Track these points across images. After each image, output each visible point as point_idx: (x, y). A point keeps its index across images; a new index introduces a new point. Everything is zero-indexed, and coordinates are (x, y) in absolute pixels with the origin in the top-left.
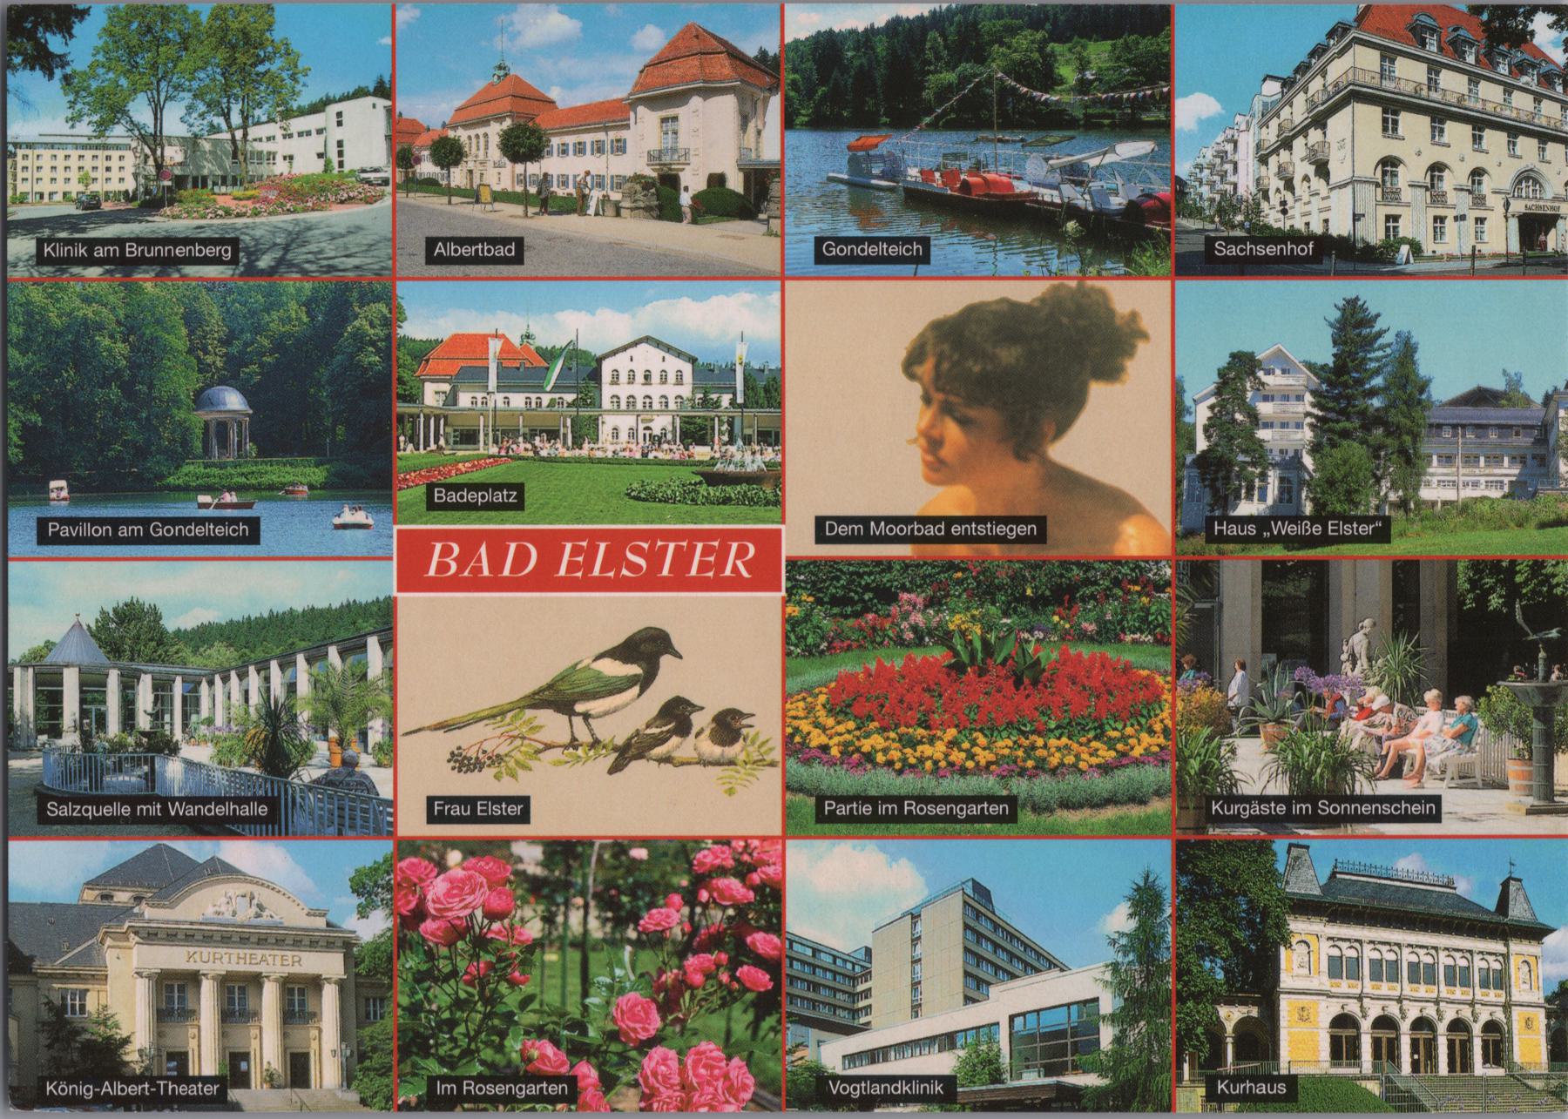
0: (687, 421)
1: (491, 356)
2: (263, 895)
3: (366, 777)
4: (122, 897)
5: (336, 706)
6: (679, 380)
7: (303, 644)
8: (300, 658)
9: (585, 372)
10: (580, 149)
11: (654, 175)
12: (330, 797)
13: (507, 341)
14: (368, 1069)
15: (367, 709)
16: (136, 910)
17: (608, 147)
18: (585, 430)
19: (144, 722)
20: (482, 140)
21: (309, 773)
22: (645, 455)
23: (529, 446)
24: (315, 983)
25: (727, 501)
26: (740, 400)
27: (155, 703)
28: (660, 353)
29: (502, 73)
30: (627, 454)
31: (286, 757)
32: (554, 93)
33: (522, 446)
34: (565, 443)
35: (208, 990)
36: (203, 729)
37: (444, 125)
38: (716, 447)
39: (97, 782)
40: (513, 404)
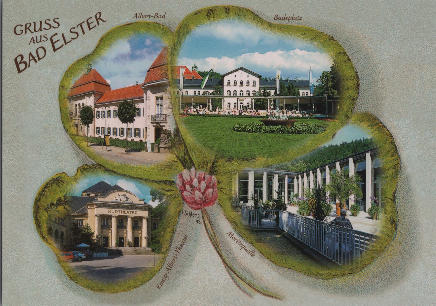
0: (257, 100)
1: (181, 75)
3: (348, 221)
5: (338, 188)
6: (254, 85)
7: (328, 161)
8: (327, 167)
9: (217, 81)
12: (337, 229)
13: (187, 70)
15: (349, 190)
18: (217, 104)
19: (275, 196)
21: (330, 219)
22: (240, 114)
23: (195, 110)
25: (273, 132)
26: (278, 92)
27: (279, 187)
28: (246, 74)
30: (233, 113)
31: (322, 212)
33: (193, 110)
34: (209, 109)
36: (295, 199)
38: (269, 111)
39: (259, 223)
40: (189, 94)
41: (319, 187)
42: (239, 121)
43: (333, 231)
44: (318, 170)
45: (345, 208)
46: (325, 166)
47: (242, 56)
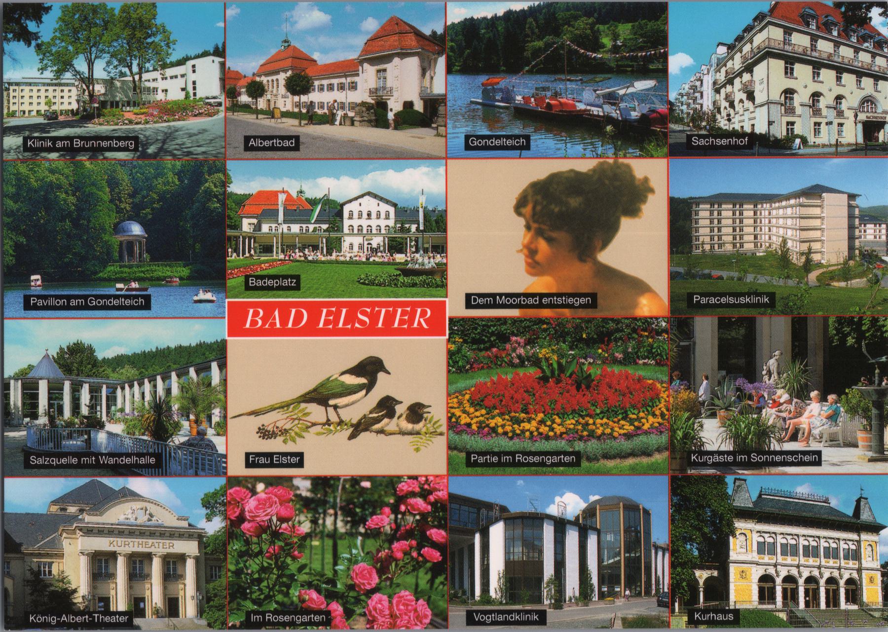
0: (392, 240)
1: (280, 203)
2: (152, 508)
4: (72, 510)
5: (194, 401)
6: (387, 217)
7: (175, 366)
9: (333, 212)
10: (331, 88)
11: (373, 102)
13: (289, 196)
14: (212, 606)
15: (211, 403)
16: (80, 517)
17: (347, 86)
18: (334, 245)
19: (85, 411)
20: (275, 83)
21: (179, 439)
22: (368, 259)
23: (302, 254)
24: (182, 558)
25: (414, 285)
26: (422, 228)
27: (91, 399)
28: (374, 202)
29: (286, 44)
30: (357, 258)
31: (166, 431)
32: (316, 56)
33: (298, 254)
35: (121, 564)
36: (118, 415)
37: (254, 74)
39: (58, 445)
41: (160, 399)
42: (367, 270)
43: (185, 455)
44: (159, 378)
45: (204, 425)
46: (170, 372)
47: (370, 175)
